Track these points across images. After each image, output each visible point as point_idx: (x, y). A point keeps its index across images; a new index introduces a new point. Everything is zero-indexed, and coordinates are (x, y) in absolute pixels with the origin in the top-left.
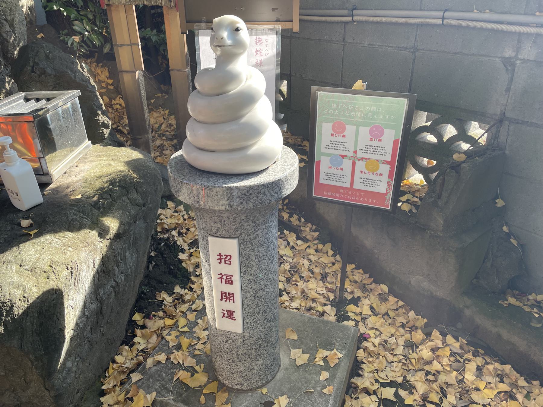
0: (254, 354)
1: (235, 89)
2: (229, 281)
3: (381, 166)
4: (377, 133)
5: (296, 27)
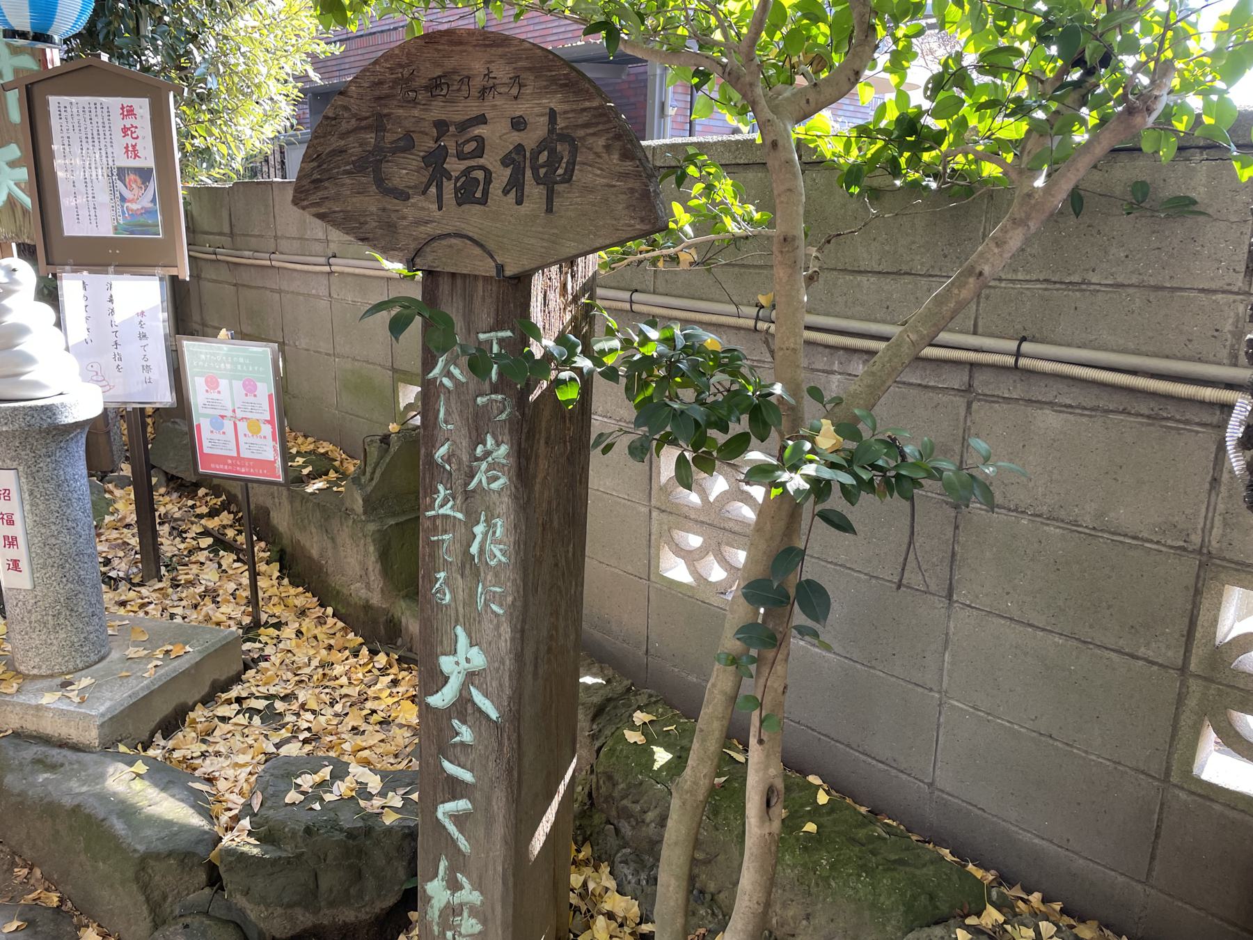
0: (51, 622)
1: (9, 319)
2: (11, 522)
3: (263, 426)
4: (250, 388)
5: (185, 274)
